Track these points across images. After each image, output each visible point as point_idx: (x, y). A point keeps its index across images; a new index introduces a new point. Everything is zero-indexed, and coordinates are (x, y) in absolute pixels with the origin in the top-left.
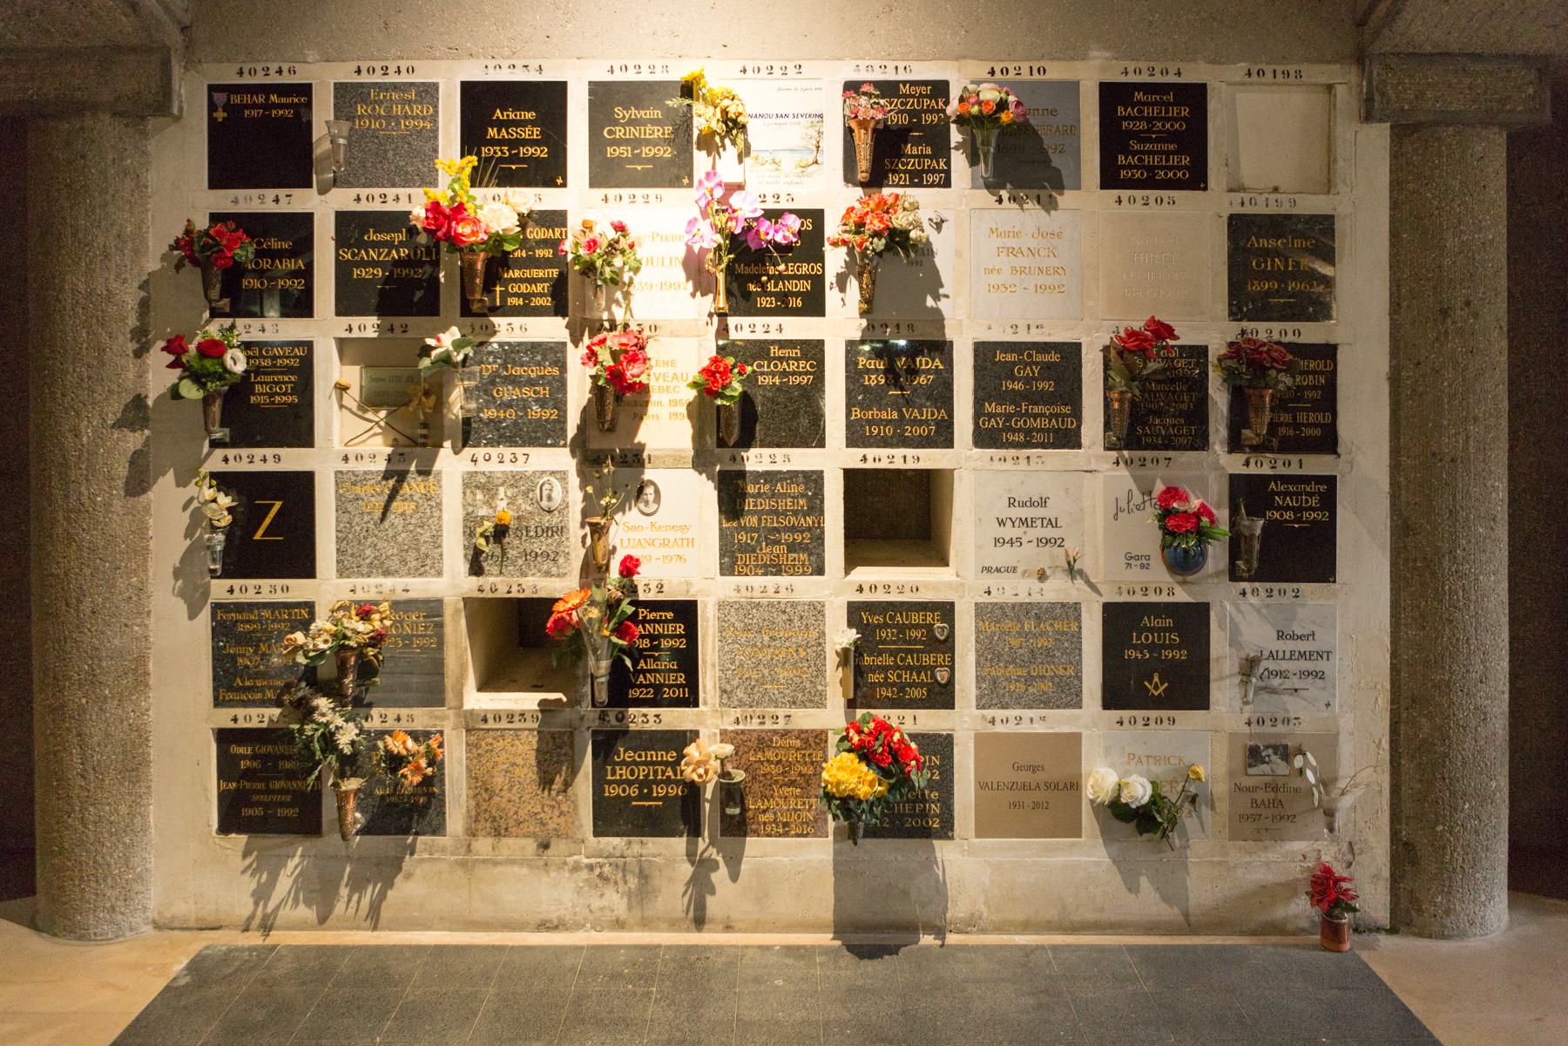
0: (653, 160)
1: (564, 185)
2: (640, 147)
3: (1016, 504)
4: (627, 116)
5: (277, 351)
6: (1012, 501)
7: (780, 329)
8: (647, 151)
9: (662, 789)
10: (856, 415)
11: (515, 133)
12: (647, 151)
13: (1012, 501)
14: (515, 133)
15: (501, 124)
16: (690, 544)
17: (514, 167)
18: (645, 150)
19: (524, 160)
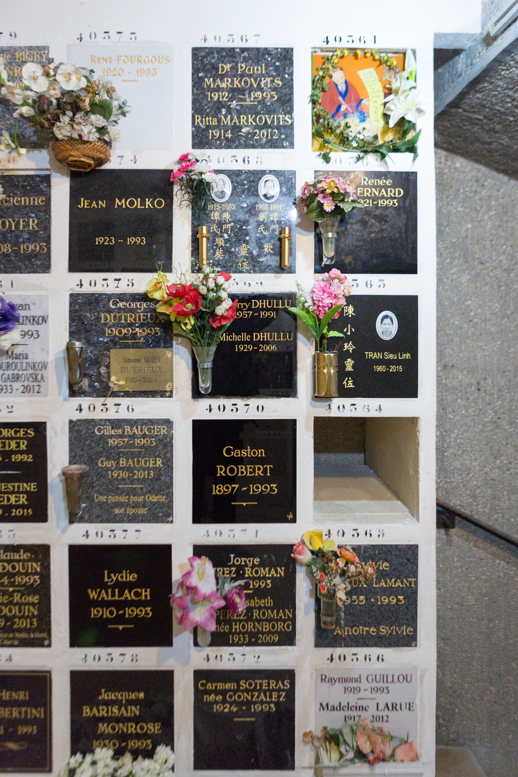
0: (135, 620)
1: (294, 520)
2: (123, 609)
3: (327, 680)
4: (115, 579)
5: (108, 431)
6: (324, 677)
7: (10, 659)
8: (129, 612)
9: (256, 583)
10: (87, 713)
11: (245, 471)
12: (129, 612)
13: (324, 677)
14: (245, 471)
15: (227, 462)
16: (394, 705)
17: (244, 504)
18: (128, 611)
19: (253, 498)
